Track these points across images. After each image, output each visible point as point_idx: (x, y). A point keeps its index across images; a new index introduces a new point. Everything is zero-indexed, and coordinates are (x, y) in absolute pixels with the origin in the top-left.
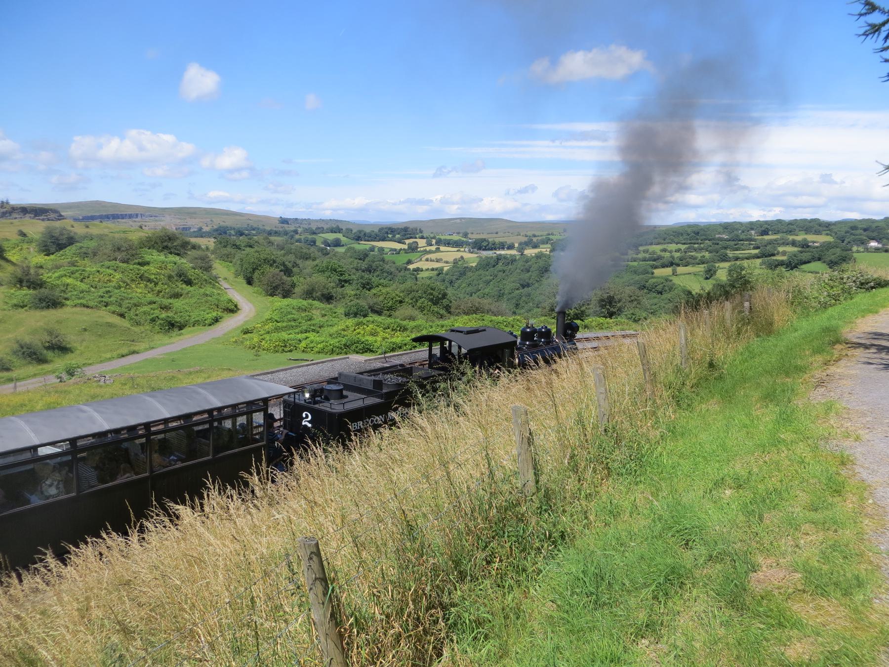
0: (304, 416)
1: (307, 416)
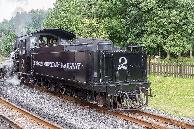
0: (120, 61)
1: (123, 61)
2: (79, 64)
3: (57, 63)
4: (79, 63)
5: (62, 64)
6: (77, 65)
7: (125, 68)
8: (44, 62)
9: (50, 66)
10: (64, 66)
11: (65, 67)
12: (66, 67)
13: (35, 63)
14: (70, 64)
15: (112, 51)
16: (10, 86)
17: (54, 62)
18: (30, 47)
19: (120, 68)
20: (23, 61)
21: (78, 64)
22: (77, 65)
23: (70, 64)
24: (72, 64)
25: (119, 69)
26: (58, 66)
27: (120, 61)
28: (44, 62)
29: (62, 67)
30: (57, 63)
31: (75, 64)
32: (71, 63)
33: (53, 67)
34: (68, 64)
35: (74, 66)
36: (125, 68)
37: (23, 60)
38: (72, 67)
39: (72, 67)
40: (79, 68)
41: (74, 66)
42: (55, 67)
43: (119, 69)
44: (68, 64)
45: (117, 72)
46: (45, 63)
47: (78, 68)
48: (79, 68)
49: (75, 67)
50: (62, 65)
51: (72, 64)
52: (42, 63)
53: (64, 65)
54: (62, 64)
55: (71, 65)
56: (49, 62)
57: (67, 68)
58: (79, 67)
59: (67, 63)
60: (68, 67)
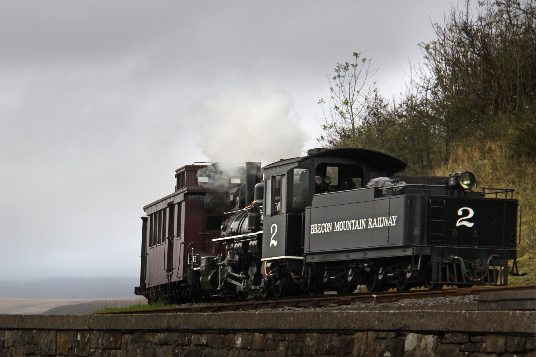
0: (460, 213)
1: (466, 213)
2: (395, 218)
3: (360, 220)
4: (395, 215)
5: (370, 222)
6: (392, 218)
7: (470, 225)
8: (335, 223)
9: (348, 229)
10: (374, 224)
11: (375, 225)
12: (376, 225)
13: (312, 229)
14: (382, 219)
15: (450, 197)
16: (204, 329)
17: (355, 221)
18: (404, 345)
19: (460, 224)
20: (274, 227)
21: (393, 217)
22: (392, 218)
23: (382, 219)
24: (385, 219)
25: (458, 224)
26: (363, 225)
27: (460, 213)
28: (335, 223)
29: (370, 226)
30: (362, 221)
31: (389, 218)
32: (383, 218)
33: (353, 229)
34: (380, 219)
35: (389, 220)
36: (470, 225)
37: (274, 227)
38: (385, 223)
39: (385, 223)
40: (394, 223)
41: (389, 220)
42: (357, 229)
43: (458, 224)
44: (380, 219)
45: (454, 230)
46: (338, 224)
47: (393, 224)
48: (394, 223)
49: (390, 222)
50: (370, 223)
51: (385, 219)
52: (329, 225)
53: (372, 223)
54: (370, 222)
55: (384, 220)
56: (345, 221)
57: (378, 226)
58: (394, 221)
59: (379, 218)
60: (379, 225)
